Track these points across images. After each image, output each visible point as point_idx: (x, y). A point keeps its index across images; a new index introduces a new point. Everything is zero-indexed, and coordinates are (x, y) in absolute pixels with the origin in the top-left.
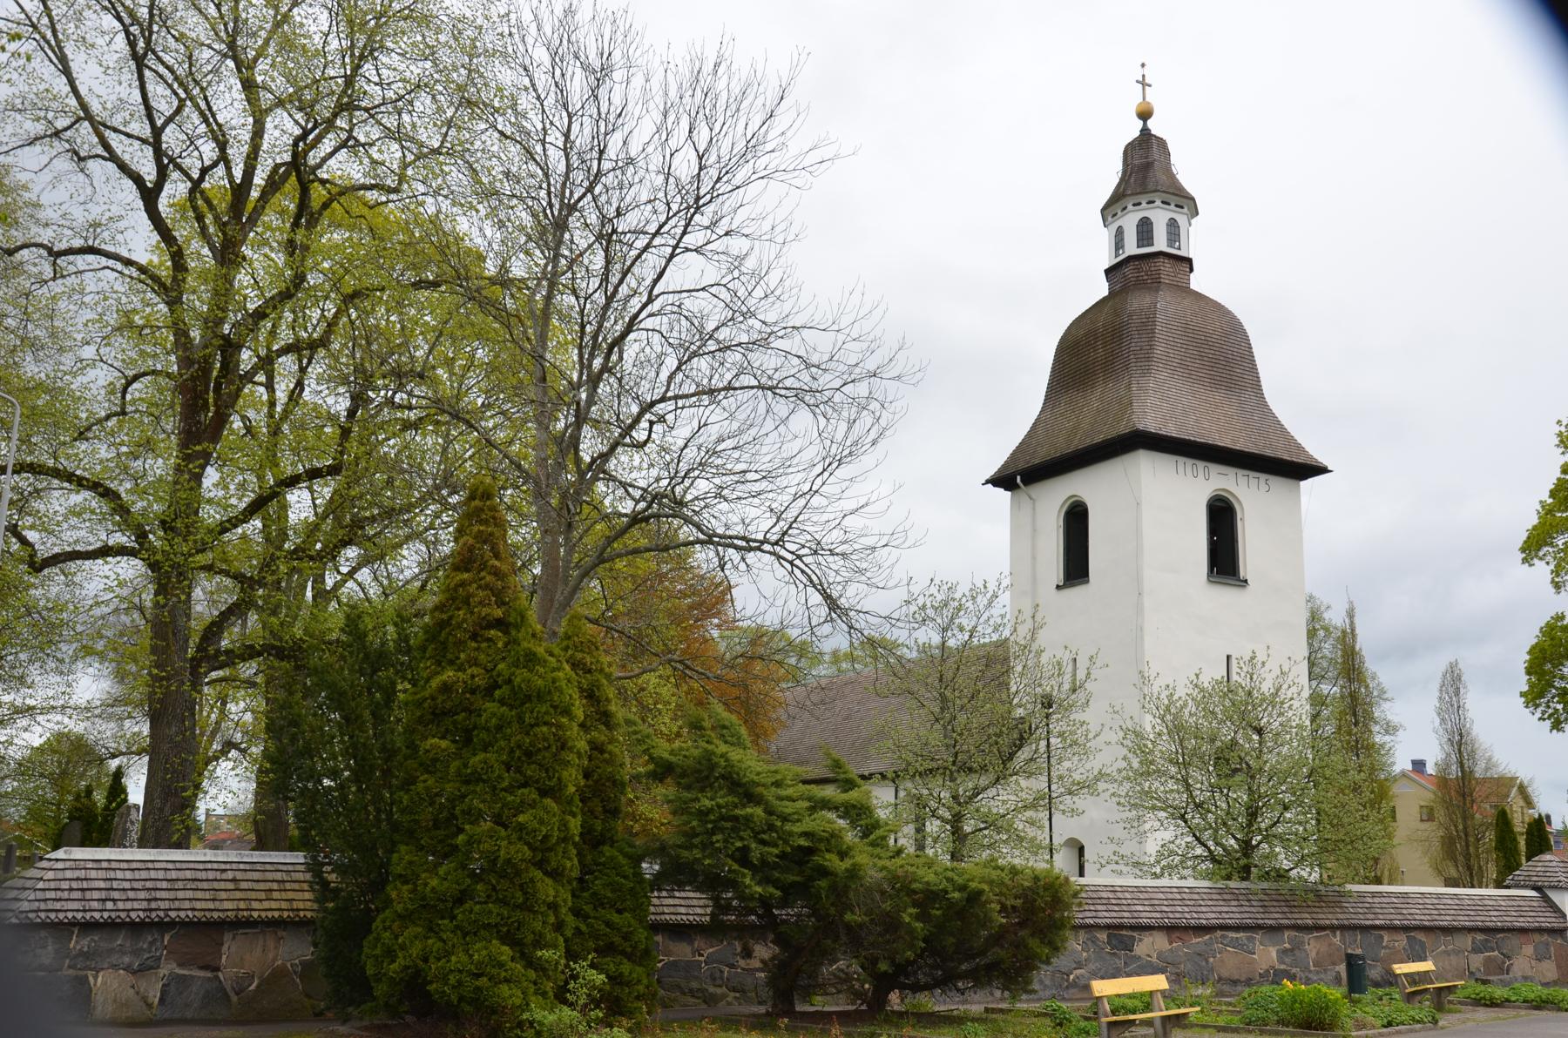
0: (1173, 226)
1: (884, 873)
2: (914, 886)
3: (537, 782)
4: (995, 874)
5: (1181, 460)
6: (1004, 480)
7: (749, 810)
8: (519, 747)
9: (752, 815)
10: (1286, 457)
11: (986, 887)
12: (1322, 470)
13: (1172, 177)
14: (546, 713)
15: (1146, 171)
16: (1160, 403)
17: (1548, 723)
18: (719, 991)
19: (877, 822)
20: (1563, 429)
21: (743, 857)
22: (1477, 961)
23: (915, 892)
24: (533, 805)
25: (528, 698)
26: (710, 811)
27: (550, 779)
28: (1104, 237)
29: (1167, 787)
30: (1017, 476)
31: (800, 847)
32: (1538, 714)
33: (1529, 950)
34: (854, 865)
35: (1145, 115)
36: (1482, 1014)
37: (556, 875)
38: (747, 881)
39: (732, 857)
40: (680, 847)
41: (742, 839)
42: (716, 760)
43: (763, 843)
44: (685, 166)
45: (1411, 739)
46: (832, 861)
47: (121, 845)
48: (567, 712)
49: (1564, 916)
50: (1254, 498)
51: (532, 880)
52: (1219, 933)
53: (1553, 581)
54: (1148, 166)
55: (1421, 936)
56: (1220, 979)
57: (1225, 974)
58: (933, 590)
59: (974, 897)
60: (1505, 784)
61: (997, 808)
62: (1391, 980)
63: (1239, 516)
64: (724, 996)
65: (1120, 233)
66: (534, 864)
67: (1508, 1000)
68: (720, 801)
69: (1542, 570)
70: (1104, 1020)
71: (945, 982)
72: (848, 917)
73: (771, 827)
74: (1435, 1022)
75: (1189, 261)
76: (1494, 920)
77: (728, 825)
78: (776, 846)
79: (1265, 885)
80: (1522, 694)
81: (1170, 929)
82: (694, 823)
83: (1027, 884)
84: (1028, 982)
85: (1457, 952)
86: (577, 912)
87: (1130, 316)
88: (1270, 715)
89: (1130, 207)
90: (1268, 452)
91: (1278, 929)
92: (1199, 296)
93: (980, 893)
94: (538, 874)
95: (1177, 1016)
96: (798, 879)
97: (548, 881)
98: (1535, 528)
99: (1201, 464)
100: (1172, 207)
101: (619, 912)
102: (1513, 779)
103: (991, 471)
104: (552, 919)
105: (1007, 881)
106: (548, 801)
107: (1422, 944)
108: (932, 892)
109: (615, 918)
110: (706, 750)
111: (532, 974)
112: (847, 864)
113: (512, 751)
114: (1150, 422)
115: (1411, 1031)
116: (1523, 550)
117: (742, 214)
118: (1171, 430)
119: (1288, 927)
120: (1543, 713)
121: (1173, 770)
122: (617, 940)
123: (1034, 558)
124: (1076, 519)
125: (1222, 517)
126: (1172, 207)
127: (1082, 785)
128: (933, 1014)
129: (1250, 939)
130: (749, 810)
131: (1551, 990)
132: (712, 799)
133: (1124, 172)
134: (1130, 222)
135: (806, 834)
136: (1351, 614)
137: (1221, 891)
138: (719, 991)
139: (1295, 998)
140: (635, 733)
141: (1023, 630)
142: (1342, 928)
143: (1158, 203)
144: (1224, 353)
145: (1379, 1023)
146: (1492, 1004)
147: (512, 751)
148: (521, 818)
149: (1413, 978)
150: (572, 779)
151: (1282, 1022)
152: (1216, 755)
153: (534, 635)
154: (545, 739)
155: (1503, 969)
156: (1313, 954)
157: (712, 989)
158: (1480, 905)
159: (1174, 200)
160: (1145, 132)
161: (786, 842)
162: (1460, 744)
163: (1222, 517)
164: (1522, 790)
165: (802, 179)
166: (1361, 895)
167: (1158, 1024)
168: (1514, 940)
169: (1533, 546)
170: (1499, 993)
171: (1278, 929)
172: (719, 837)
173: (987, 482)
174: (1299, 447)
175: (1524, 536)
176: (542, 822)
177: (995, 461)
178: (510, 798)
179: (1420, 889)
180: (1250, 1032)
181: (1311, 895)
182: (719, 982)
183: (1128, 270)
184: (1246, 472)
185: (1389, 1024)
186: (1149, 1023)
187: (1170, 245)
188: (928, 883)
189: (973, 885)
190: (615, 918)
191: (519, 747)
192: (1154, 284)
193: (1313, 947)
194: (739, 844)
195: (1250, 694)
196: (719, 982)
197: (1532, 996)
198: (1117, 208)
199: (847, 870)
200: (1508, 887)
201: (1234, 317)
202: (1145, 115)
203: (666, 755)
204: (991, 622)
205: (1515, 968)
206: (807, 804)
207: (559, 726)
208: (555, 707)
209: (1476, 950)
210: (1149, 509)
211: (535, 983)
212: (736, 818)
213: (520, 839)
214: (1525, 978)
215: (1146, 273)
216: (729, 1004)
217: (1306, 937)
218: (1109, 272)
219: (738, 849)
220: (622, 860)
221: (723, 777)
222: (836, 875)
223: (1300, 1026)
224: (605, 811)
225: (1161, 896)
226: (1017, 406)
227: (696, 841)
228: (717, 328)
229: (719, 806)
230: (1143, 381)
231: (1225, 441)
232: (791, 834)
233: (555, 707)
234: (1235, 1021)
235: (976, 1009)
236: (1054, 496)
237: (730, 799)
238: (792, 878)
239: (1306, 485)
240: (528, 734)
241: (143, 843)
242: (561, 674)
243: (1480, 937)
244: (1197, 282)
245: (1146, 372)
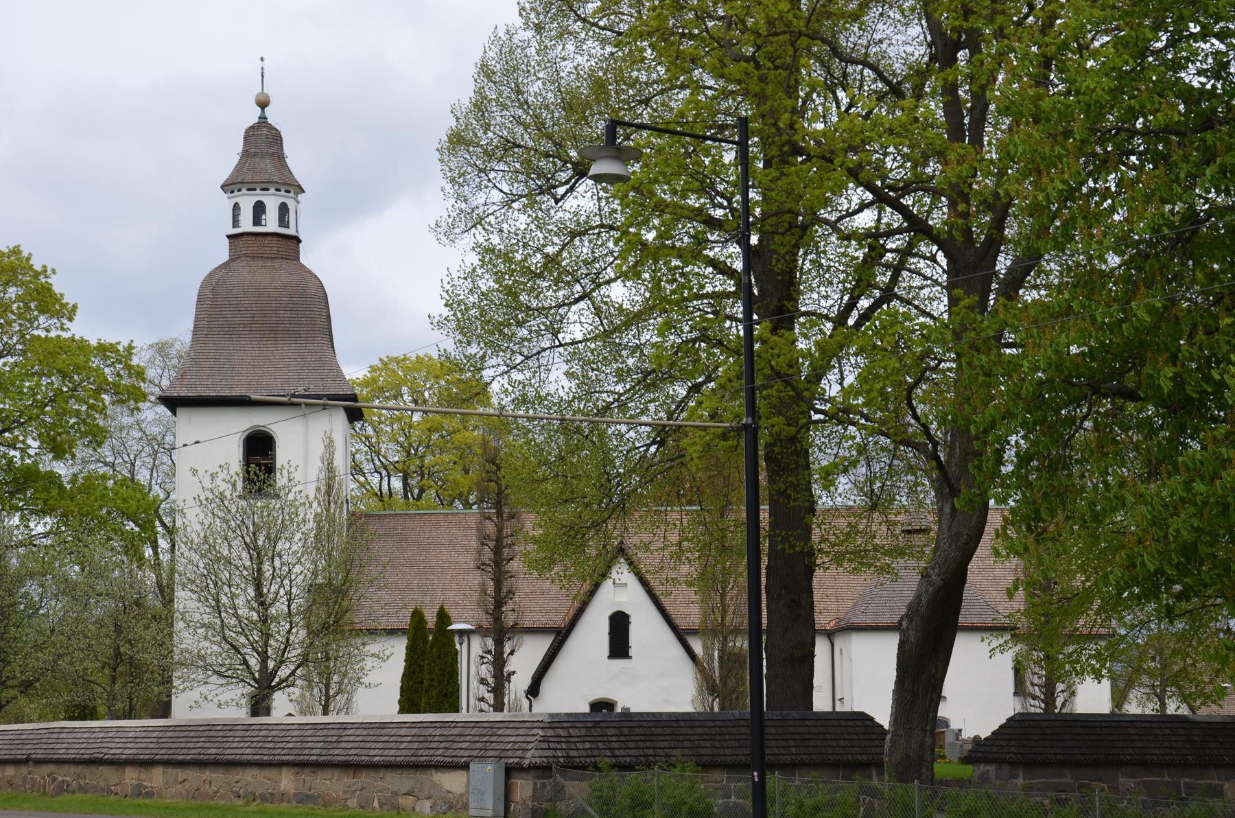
0: (283, 209)
15: (263, 144)
28: (225, 203)
35: (263, 104)
65: (236, 208)
76: (115, 750)
100: (283, 193)
134: (247, 202)
143: (272, 191)
160: (263, 118)
183: (241, 241)
202: (263, 104)
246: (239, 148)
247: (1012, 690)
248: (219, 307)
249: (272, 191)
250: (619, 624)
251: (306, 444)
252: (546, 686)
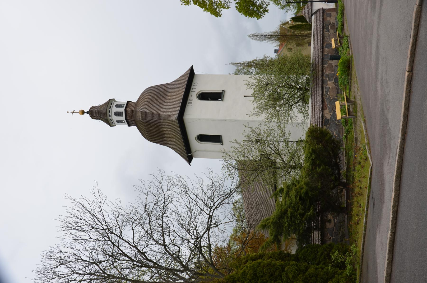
0: (117, 106)
1: (307, 177)
2: (310, 168)
3: (280, 272)
4: (307, 146)
5: (187, 107)
6: (189, 160)
7: (289, 212)
8: (270, 277)
9: (290, 212)
10: (188, 78)
11: (311, 148)
12: (192, 68)
13: (102, 106)
14: (260, 269)
15: (100, 113)
16: (170, 112)
17: (266, 13)
18: (341, 233)
19: (292, 183)
20: (184, 4)
21: (302, 215)
22: (331, 31)
23: (312, 168)
24: (287, 274)
25: (255, 274)
26: (289, 224)
27: (279, 269)
28: (119, 127)
29: (283, 110)
30: (188, 155)
31: (299, 199)
32: (264, 15)
33: (328, 18)
34: (305, 184)
35: (83, 112)
36: (346, 27)
37: (307, 268)
38: (309, 214)
39: (302, 218)
40: (299, 233)
41: (297, 215)
42: (274, 221)
43: (298, 209)
44: (94, 235)
45: (269, 50)
46: (303, 191)
47: (311, 33)
48: (260, 263)
49: (319, 9)
50: (199, 87)
51: (309, 274)
52: (324, 96)
53: (227, 9)
54: (99, 112)
55: (325, 44)
56: (337, 96)
57: (335, 95)
58: (224, 171)
59: (314, 151)
60: (281, 28)
61: (288, 155)
62: (336, 49)
63: (204, 92)
64: (342, 232)
65: (118, 121)
66: (304, 274)
67: (342, 22)
68: (286, 220)
69: (224, 11)
70: (348, 116)
71: (337, 166)
72: (319, 187)
73: (294, 207)
74: (348, 36)
75: (128, 102)
76: (320, 26)
77: (293, 219)
78: (299, 206)
79: (311, 84)
80: (258, 19)
81: (323, 109)
82: (292, 228)
83: (310, 138)
84: (337, 141)
85: (329, 36)
86: (318, 264)
87: (143, 119)
88: (263, 81)
90: (186, 82)
91: (323, 81)
92: (139, 100)
93: (312, 149)
94: (307, 273)
95: (347, 98)
96: (308, 201)
97: (309, 270)
98: (211, 13)
99: (188, 101)
100: (112, 106)
101: (318, 252)
102: (280, 26)
103: (186, 163)
104: (320, 269)
105: (309, 143)
106: (286, 269)
107: (327, 44)
108: (312, 163)
109: (319, 253)
110: (272, 223)
111: (336, 276)
112: (305, 187)
113: (271, 279)
114: (176, 115)
115: (350, 42)
116: (217, 16)
117: (111, 217)
118: (178, 109)
119: (322, 78)
120: (263, 14)
121: (277, 108)
122: (326, 253)
123: (213, 151)
124: (202, 138)
125: (204, 96)
126: (112, 106)
127: (282, 131)
128: (347, 169)
129: (326, 88)
130: (289, 212)
131: (339, 12)
132: (286, 223)
133: (100, 119)
134: (115, 118)
135: (296, 198)
136: (233, 64)
137: (312, 95)
138: (341, 233)
139: (342, 70)
140: (266, 246)
141: (237, 146)
142: (323, 64)
143: (110, 110)
144: (156, 94)
145: (348, 50)
146: (343, 25)
147: (271, 279)
148: (291, 277)
149: (336, 44)
150: (278, 263)
151: (348, 75)
152: (274, 99)
153: (237, 273)
154: (267, 270)
155: (334, 25)
156: (330, 72)
157: (340, 235)
158: (316, 30)
159: (109, 105)
160: (88, 113)
161: (298, 203)
162: (271, 36)
163: (204, 96)
164: (284, 24)
165: (103, 198)
166: (313, 59)
167: (349, 104)
168: (326, 22)
169: (216, 13)
170: (340, 24)
171: (323, 81)
172: (296, 221)
173: (190, 164)
174: (185, 74)
175: (213, 16)
176: (292, 271)
177: (183, 161)
178: (285, 280)
179: (311, 51)
180: (351, 82)
181: (314, 72)
182: (338, 233)
183: (129, 120)
184: (191, 89)
185: (349, 47)
186: (349, 106)
187: (123, 107)
188: (310, 164)
189: (310, 151)
190: (319, 253)
191: (270, 277)
192: (134, 112)
193: (328, 72)
194: (298, 216)
195: (257, 86)
196: (338, 233)
197: (340, 16)
198: (110, 122)
199: (306, 186)
200: (311, 23)
201: (146, 90)
202: (83, 112)
203: (273, 237)
204: (234, 155)
205: (333, 22)
206: (287, 198)
207: (264, 266)
208: (258, 267)
209: (329, 31)
210: (201, 116)
211: (339, 275)
212: (291, 217)
213: (297, 277)
214: (336, 19)
215: (131, 115)
216: (344, 230)
217: (325, 73)
218: (129, 125)
219: (300, 216)
220: (303, 251)
221: (279, 220)
222: (307, 190)
223: (349, 69)
224: (288, 256)
225: (313, 111)
226: (168, 157)
227: (297, 228)
228: (144, 230)
229: (288, 221)
230: (162, 117)
231: (182, 94)
232: (295, 202)
233: (258, 267)
234: (348, 87)
235: (345, 159)
237: (285, 218)
238: (308, 203)
239: (196, 72)
240: (266, 275)
241: (311, 30)
242: (248, 265)
243: (325, 30)
244: (134, 100)
245: (160, 115)
246: (98, 121)
248: (154, 132)
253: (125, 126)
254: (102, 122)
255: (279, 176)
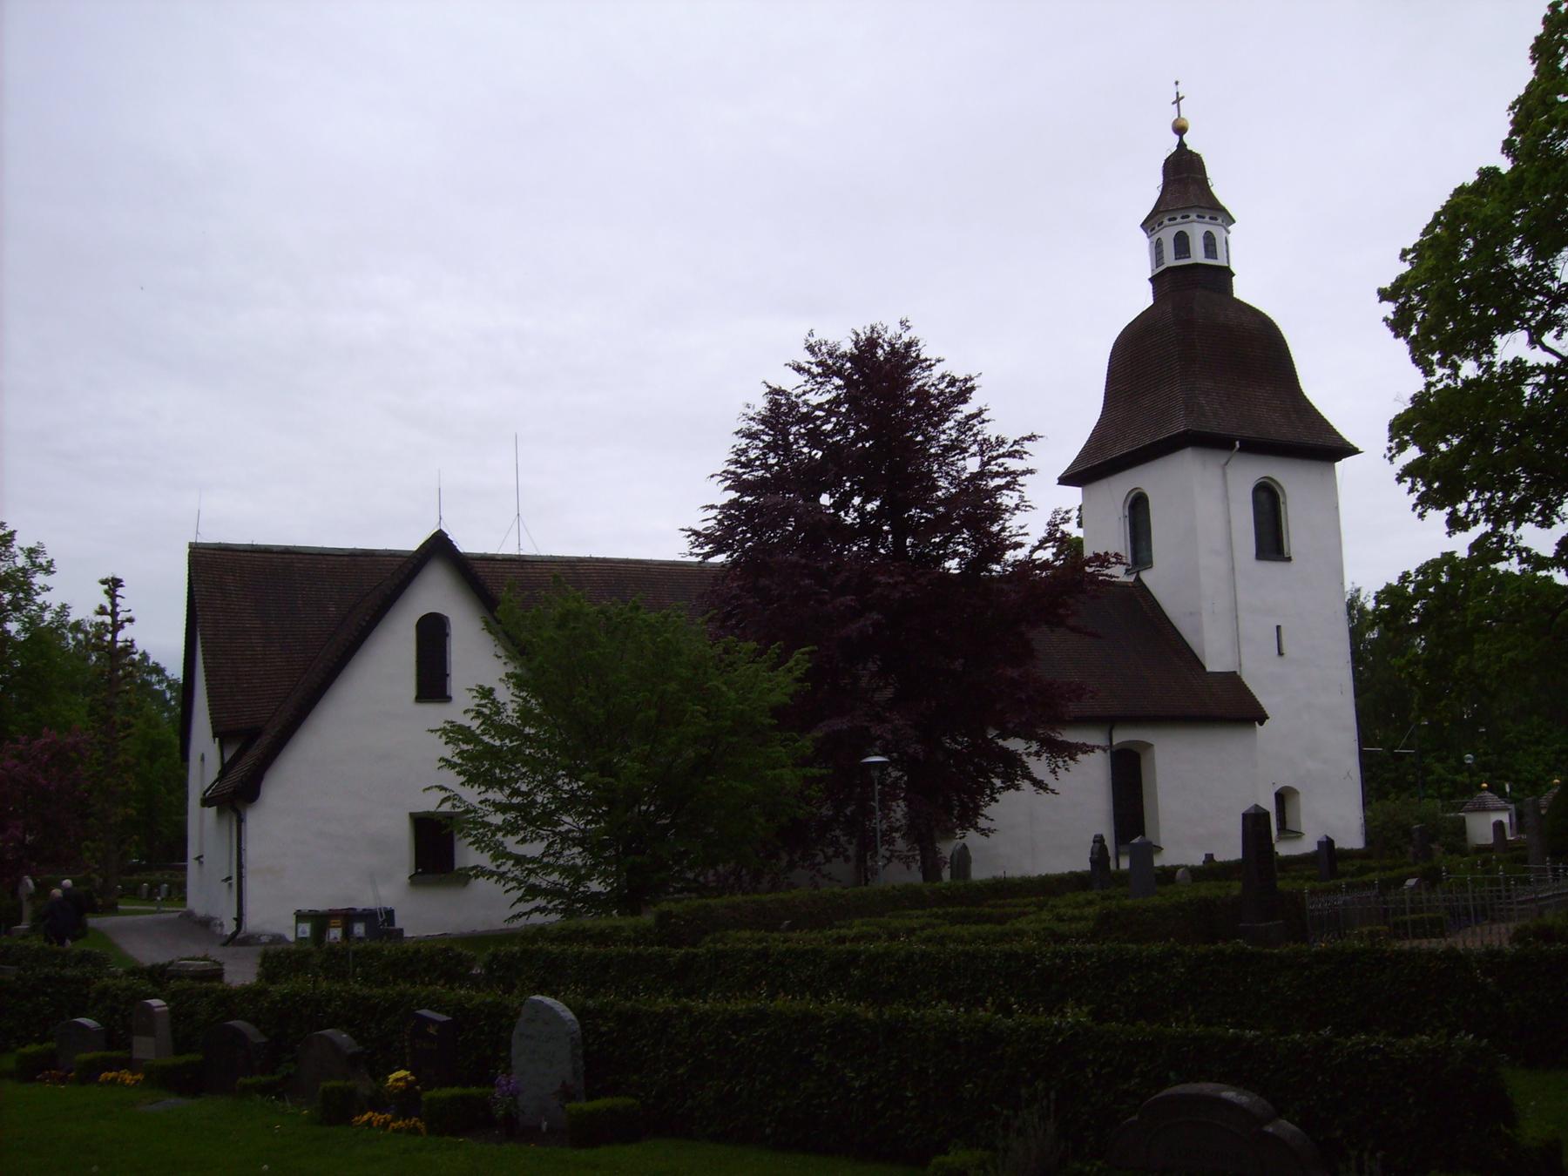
12: (1354, 451)
15: (1185, 179)
35: (1180, 130)
50: (1293, 479)
89: (1166, 222)
124: (1138, 507)
125: (1268, 501)
134: (1168, 235)
143: (1193, 217)
160: (1181, 145)
163: (1268, 501)
187: (1207, 256)
202: (1180, 130)
236: (1117, 489)
244: (1244, 290)
246: (1159, 180)
247: (413, 693)
248: (1138, 359)
249: (1193, 217)
250: (433, 633)
251: (1226, 497)
252: (1285, 649)
253: (1146, 269)
254: (1155, 195)
255: (1118, 573)
